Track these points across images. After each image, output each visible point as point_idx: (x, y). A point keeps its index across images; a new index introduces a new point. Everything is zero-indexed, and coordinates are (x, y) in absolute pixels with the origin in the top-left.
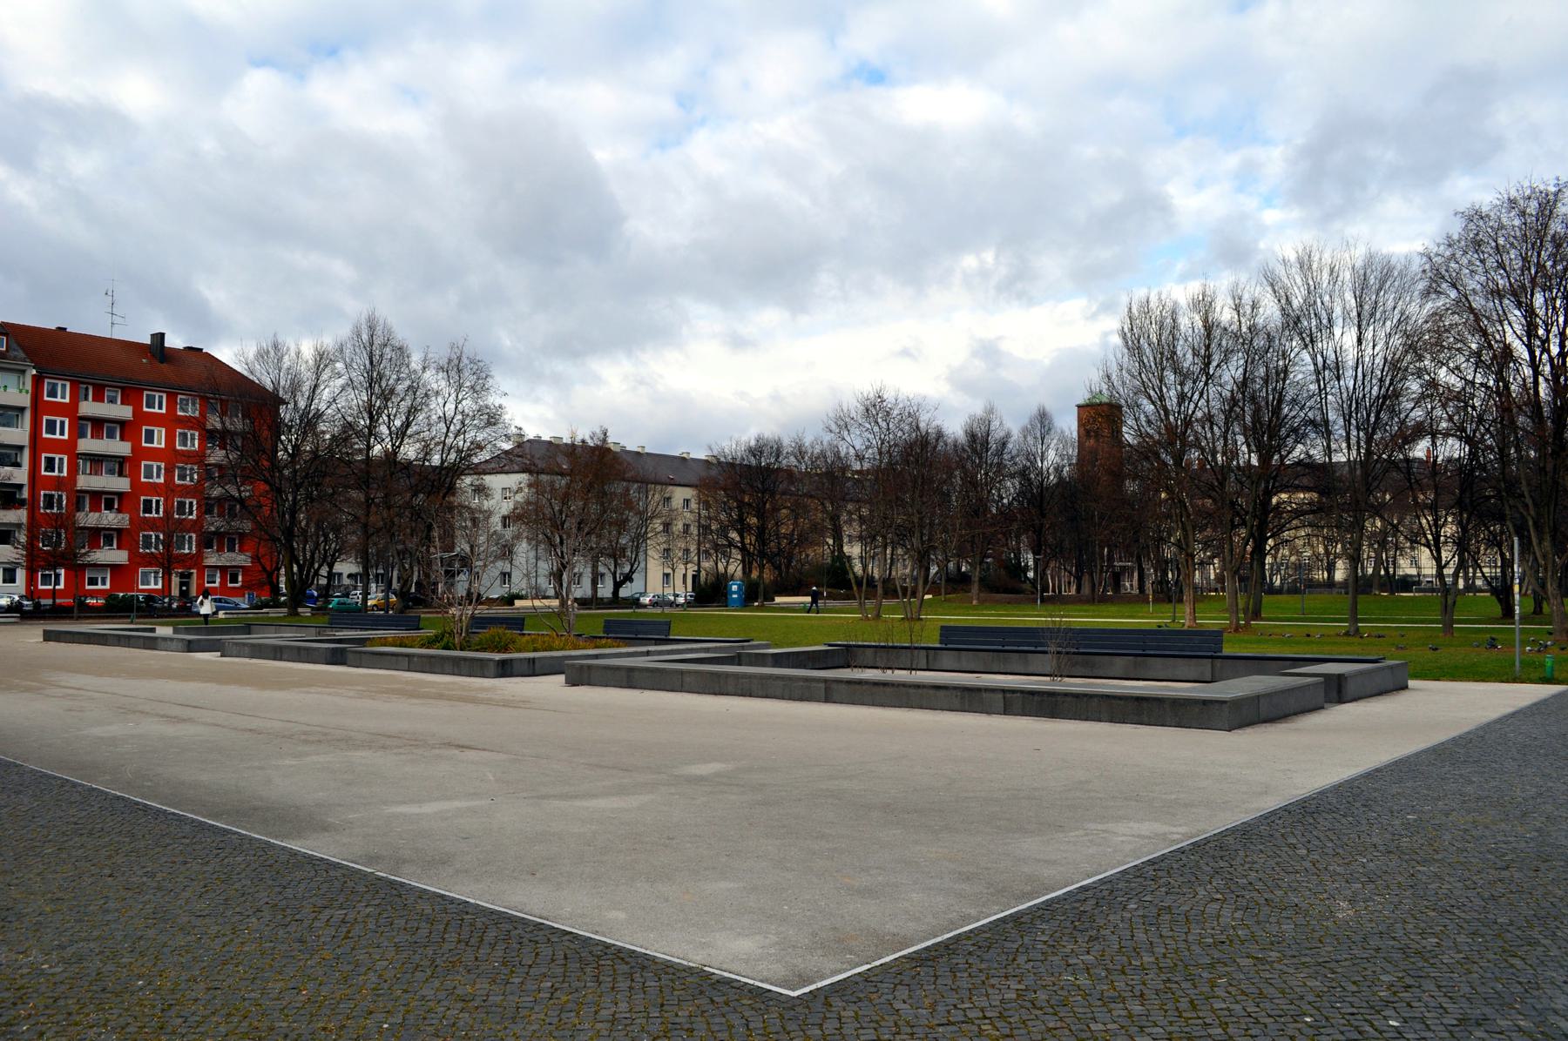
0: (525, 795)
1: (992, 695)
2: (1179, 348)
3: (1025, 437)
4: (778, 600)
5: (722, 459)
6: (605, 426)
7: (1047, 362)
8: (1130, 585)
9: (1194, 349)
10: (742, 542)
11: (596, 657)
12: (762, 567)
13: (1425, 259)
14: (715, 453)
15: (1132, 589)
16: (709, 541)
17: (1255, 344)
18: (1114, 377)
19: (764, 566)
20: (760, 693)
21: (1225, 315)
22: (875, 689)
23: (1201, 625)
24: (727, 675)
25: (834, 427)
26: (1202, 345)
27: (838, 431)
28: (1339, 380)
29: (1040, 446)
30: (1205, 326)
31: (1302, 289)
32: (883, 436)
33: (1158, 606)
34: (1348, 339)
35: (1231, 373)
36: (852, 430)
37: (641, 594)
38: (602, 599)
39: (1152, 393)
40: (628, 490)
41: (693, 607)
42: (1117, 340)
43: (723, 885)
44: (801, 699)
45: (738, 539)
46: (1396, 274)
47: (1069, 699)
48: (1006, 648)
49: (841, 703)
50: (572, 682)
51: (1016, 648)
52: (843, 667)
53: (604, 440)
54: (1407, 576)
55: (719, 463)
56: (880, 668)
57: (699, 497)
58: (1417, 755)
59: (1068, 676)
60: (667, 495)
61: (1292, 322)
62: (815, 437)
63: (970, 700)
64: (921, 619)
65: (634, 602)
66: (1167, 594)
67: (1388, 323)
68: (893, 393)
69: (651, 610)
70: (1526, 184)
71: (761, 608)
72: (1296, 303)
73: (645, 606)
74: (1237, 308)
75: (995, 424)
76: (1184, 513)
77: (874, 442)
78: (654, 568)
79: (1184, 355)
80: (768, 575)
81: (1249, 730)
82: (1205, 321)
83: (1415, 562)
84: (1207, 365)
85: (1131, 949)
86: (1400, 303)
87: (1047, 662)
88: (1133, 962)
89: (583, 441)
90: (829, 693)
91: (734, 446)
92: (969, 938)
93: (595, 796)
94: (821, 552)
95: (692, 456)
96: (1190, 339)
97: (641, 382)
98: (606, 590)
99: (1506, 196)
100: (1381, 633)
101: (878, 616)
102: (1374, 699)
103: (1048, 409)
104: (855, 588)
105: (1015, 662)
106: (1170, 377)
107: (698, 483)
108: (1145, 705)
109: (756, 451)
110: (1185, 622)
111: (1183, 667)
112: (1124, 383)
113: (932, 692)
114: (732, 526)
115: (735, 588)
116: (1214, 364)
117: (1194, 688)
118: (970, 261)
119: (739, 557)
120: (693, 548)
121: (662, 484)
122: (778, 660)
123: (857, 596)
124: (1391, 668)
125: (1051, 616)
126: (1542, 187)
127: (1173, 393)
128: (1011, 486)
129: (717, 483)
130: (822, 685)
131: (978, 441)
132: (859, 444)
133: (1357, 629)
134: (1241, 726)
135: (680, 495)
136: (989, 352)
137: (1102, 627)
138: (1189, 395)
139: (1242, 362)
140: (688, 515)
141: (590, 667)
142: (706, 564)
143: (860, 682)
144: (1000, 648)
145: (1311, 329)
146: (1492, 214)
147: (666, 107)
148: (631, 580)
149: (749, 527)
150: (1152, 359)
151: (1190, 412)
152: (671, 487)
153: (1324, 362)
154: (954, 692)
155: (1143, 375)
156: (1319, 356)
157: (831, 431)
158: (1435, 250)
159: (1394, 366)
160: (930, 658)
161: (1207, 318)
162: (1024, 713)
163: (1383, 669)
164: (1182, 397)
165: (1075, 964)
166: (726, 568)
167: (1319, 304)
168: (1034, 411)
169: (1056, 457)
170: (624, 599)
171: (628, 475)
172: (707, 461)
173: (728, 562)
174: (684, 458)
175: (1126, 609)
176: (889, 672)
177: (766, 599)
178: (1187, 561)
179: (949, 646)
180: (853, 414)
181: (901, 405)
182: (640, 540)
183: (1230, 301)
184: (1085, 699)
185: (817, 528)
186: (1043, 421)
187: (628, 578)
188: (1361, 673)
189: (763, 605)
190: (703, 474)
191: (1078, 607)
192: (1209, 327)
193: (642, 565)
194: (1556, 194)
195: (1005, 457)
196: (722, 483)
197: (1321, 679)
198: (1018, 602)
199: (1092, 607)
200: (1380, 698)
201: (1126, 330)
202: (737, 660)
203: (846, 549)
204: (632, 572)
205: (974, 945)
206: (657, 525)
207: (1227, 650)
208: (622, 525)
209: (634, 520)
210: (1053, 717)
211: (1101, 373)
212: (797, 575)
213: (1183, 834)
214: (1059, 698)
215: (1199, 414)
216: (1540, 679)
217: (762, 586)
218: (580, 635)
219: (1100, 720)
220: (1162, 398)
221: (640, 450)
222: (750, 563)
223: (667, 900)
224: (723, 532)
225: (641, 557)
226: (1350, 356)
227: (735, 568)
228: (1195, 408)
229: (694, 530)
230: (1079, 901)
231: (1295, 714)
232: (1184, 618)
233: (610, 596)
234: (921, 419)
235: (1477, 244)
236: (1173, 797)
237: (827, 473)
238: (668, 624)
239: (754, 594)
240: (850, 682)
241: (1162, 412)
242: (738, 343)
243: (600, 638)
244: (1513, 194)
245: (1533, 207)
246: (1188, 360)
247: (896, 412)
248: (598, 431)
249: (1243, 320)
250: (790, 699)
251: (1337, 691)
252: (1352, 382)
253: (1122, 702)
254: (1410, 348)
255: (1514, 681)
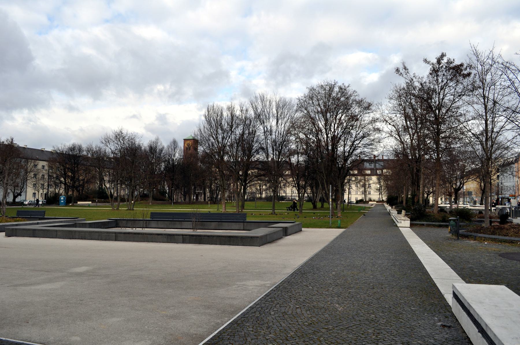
0: (7, 285)
1: (178, 237)
2: (223, 122)
3: (168, 149)
4: (79, 203)
5: (59, 152)
6: (13, 137)
7: (179, 124)
8: (201, 198)
9: (228, 123)
10: (65, 182)
11: (17, 225)
12: (73, 191)
13: (298, 100)
14: (56, 149)
15: (201, 200)
16: (53, 181)
17: (246, 122)
18: (202, 130)
19: (74, 191)
20: (89, 238)
21: (238, 113)
22: (135, 236)
23: (228, 211)
24: (75, 231)
25: (104, 142)
26: (230, 122)
27: (105, 143)
28: (271, 135)
29: (173, 152)
30: (231, 116)
31: (261, 106)
32: (121, 146)
33: (211, 205)
34: (274, 123)
35: (239, 131)
36: (111, 143)
37: (24, 200)
38: (8, 202)
39: (214, 136)
40: (21, 161)
41: (46, 205)
42: (203, 118)
43: (115, 320)
44: (106, 240)
45: (64, 181)
46: (288, 104)
47: (206, 237)
48: (174, 220)
49: (121, 241)
50: (8, 235)
51: (177, 220)
52: (114, 227)
53: (12, 142)
54: (283, 196)
55: (57, 153)
56: (131, 227)
57: (49, 165)
58: (320, 252)
59: (199, 229)
60: (36, 164)
61: (258, 116)
62: (96, 144)
63: (171, 239)
64: (134, 210)
65: (21, 204)
66: (214, 201)
67: (285, 119)
68: (126, 131)
69: (28, 206)
70: (326, 81)
71: (72, 206)
72: (259, 111)
73: (26, 205)
74: (242, 111)
75: (159, 144)
76: (223, 175)
77: (118, 148)
78: (30, 190)
79: (224, 124)
80: (76, 194)
81: (265, 246)
82: (232, 114)
83: (285, 192)
84: (232, 128)
85: (284, 330)
86: (289, 113)
87: (189, 225)
88: (288, 336)
89: (3, 142)
90: (117, 237)
91: (63, 147)
92: (224, 333)
93: (39, 284)
94: (96, 186)
95: (46, 150)
96: (227, 120)
97: (30, 120)
98: (10, 199)
99: (320, 84)
100: (325, 214)
101: (118, 209)
102: (295, 234)
103: (176, 139)
104: (110, 199)
105: (178, 225)
106: (220, 131)
107: (48, 160)
108: (232, 239)
109: (73, 149)
110: (222, 210)
111: (234, 225)
112: (205, 132)
113: (156, 236)
114: (62, 176)
115: (62, 198)
116: (234, 128)
117: (246, 232)
118: (160, 87)
119: (64, 187)
120: (46, 184)
121: (34, 160)
122: (91, 225)
123: (111, 202)
124: (298, 224)
125: (193, 209)
126: (330, 83)
127: (220, 136)
128: (163, 165)
129: (56, 160)
130: (114, 235)
131: (152, 149)
132: (113, 148)
133: (275, 213)
134: (262, 245)
135: (41, 164)
136: (162, 118)
137: (171, 212)
138: (226, 137)
139: (242, 128)
140: (44, 171)
141: (16, 229)
142: (51, 190)
143: (129, 233)
144: (172, 220)
145: (263, 119)
146: (317, 89)
147: (44, 19)
148: (21, 195)
149: (69, 176)
150: (214, 125)
151: (226, 143)
152: (38, 161)
153: (267, 129)
154: (164, 236)
155: (211, 130)
156: (265, 128)
157: (103, 143)
158: (301, 98)
159: (288, 132)
160: (147, 224)
161: (232, 113)
162: (190, 242)
163: (296, 225)
164: (223, 138)
165: (269, 339)
166: (59, 191)
167: (266, 111)
168: (172, 140)
169: (178, 155)
170: (17, 202)
171: (21, 156)
172: (52, 152)
173: (60, 189)
174: (43, 150)
175: (201, 206)
176: (134, 229)
177: (74, 203)
178: (223, 191)
179: (154, 219)
180: (111, 137)
181: (129, 135)
182: (25, 181)
183: (239, 108)
184: (211, 237)
185: (94, 177)
186: (175, 142)
187: (20, 194)
188: (291, 226)
189: (73, 205)
190: (51, 157)
191: (185, 206)
192: (232, 116)
193: (25, 190)
194: (334, 85)
195: (162, 155)
196: (58, 160)
197: (282, 229)
198: (164, 204)
199: (189, 206)
200: (296, 234)
201: (206, 115)
202: (74, 225)
203: (366, 183)
204: (21, 192)
205: (227, 335)
206: (32, 174)
207: (248, 219)
208: (18, 175)
209: (23, 172)
210: (200, 243)
211: (198, 128)
212: (86, 194)
213: (270, 284)
214: (202, 237)
215: (229, 144)
216: (337, 227)
217: (73, 198)
218: (7, 216)
219: (216, 244)
220: (217, 138)
221: (25, 147)
222: (68, 190)
223: (94, 329)
224: (57, 178)
225: (25, 187)
226: (274, 129)
227: (62, 191)
228: (227, 142)
229: (46, 177)
230: (253, 313)
231: (276, 240)
232: (222, 209)
233: (12, 201)
234: (136, 140)
235: (311, 98)
236: (258, 270)
237: (97, 158)
238: (44, 212)
239: (69, 201)
240: (125, 233)
241: (217, 142)
242: (71, 109)
243: (16, 217)
244: (322, 84)
245: (328, 88)
246: (226, 126)
247: (126, 138)
248: (9, 139)
249: (243, 115)
250: (101, 240)
251: (286, 232)
252: (275, 136)
253: (224, 238)
254: (293, 127)
255: (330, 228)
